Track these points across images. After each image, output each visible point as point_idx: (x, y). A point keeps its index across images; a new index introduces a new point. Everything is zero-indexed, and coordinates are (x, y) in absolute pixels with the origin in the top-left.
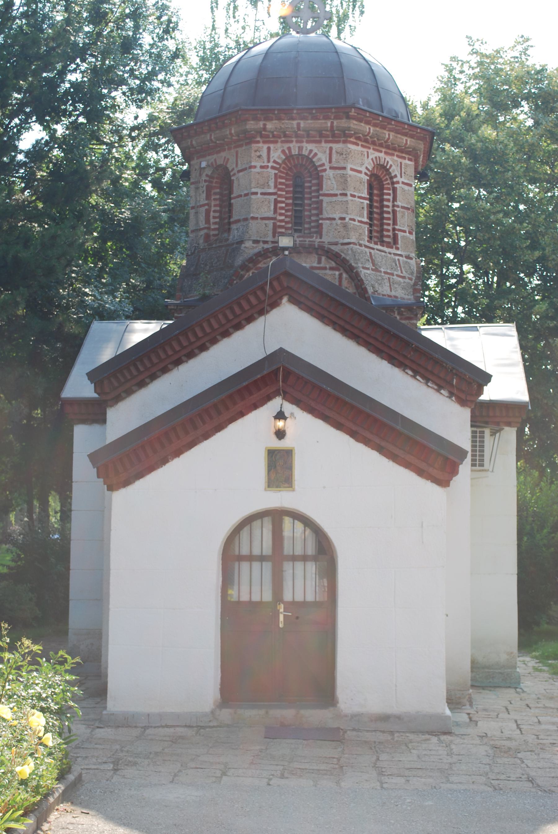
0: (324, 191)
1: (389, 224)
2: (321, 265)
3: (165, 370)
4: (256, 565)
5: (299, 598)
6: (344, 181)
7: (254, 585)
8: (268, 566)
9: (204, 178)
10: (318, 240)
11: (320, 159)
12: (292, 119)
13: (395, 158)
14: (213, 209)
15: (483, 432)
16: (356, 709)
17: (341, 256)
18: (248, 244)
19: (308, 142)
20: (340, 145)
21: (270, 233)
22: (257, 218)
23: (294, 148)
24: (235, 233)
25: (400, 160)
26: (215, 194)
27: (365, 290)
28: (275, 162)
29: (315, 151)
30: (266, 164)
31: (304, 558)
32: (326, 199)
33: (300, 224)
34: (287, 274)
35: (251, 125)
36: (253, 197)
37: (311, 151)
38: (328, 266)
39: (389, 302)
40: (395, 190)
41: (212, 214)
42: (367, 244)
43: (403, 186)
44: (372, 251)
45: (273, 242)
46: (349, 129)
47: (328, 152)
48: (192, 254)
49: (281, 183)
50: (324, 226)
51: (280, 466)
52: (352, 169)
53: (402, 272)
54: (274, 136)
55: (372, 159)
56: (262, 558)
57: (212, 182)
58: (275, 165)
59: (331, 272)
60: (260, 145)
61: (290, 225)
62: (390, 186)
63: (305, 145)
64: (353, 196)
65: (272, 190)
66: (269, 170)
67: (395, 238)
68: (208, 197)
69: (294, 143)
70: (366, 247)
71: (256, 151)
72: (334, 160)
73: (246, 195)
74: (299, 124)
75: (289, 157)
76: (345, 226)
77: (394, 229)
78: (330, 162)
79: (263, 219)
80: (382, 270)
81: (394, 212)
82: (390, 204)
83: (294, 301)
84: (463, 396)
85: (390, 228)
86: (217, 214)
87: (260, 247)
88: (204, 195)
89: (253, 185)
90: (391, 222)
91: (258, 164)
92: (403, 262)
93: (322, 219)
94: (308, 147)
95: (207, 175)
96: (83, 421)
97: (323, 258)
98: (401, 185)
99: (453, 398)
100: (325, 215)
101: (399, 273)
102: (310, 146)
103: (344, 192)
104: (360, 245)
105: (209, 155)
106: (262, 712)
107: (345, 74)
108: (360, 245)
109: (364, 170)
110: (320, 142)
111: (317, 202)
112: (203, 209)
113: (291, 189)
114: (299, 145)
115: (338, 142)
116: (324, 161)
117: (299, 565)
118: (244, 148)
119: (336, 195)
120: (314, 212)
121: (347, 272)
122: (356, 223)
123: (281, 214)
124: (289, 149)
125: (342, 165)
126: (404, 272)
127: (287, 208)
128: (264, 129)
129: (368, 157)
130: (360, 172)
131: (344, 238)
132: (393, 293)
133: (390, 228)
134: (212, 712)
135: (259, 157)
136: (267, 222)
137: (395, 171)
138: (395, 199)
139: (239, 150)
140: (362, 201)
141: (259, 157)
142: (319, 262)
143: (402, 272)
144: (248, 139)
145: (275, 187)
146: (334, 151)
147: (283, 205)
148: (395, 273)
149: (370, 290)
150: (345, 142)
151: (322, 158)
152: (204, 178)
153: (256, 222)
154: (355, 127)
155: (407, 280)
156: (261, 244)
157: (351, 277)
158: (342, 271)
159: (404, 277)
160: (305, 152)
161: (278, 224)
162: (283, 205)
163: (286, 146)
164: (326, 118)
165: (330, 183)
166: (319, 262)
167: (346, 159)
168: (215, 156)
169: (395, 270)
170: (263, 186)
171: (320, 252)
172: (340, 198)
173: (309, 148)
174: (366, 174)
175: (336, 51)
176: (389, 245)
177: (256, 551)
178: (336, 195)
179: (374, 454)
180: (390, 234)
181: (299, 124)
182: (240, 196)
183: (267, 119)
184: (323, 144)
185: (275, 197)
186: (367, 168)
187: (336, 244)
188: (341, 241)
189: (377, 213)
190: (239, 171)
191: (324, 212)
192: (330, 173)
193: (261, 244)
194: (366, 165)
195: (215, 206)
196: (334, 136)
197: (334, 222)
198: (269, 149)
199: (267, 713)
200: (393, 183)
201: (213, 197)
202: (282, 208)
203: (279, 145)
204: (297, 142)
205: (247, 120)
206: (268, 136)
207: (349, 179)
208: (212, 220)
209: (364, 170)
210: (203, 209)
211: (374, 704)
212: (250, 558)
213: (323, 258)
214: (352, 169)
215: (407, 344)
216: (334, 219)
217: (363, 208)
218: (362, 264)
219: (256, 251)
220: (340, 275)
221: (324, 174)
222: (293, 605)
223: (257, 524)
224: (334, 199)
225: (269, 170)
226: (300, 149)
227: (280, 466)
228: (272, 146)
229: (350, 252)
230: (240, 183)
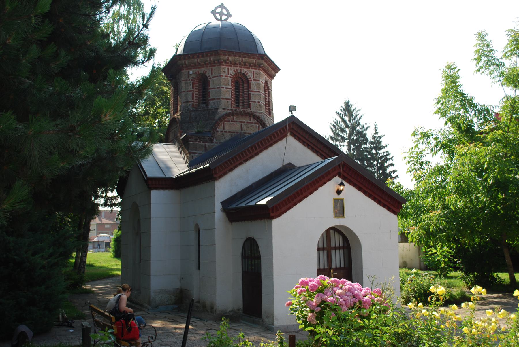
3: (241, 164)
5: (338, 266)
9: (191, 78)
11: (249, 76)
12: (240, 57)
14: (195, 93)
18: (221, 110)
19: (244, 68)
20: (257, 71)
23: (239, 69)
24: (212, 104)
26: (196, 86)
29: (247, 72)
31: (339, 248)
35: (222, 57)
41: (195, 95)
46: (262, 64)
48: (185, 112)
50: (252, 105)
51: (339, 208)
54: (231, 63)
59: (255, 125)
60: (225, 66)
63: (243, 68)
65: (230, 87)
68: (193, 88)
74: (242, 59)
75: (237, 73)
79: (227, 99)
86: (197, 96)
87: (225, 112)
88: (191, 86)
89: (222, 84)
91: (224, 75)
94: (245, 70)
95: (193, 78)
96: (156, 188)
97: (252, 118)
102: (245, 70)
105: (194, 68)
110: (249, 68)
112: (191, 93)
115: (256, 69)
117: (337, 251)
118: (216, 67)
125: (258, 79)
128: (228, 60)
139: (213, 68)
141: (224, 72)
142: (250, 120)
144: (219, 63)
150: (259, 69)
151: (250, 75)
152: (191, 78)
160: (243, 72)
163: (235, 68)
164: (254, 58)
165: (253, 86)
166: (250, 120)
167: (259, 77)
170: (226, 85)
172: (257, 93)
177: (337, 245)
179: (372, 201)
181: (242, 59)
183: (230, 55)
184: (250, 69)
187: (257, 113)
190: (213, 77)
196: (255, 66)
198: (228, 69)
203: (232, 67)
205: (221, 55)
206: (228, 63)
208: (195, 98)
210: (191, 93)
213: (252, 118)
219: (225, 113)
220: (259, 126)
224: (255, 93)
226: (241, 70)
227: (339, 208)
230: (213, 83)
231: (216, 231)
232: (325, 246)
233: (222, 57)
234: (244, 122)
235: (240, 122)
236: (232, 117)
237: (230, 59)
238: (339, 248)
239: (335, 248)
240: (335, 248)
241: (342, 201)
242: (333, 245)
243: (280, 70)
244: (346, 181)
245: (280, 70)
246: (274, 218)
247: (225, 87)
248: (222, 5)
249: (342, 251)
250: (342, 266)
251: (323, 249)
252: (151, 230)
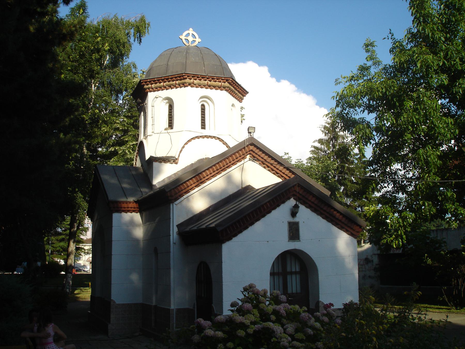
31: (296, 273)
51: (294, 232)
164: (173, 81)
177: (293, 270)
181: (208, 82)
227: (294, 232)
231: (172, 254)
232: (280, 271)
237: (195, 82)
238: (296, 273)
239: (291, 273)
241: (297, 224)
242: (289, 269)
243: (248, 93)
244: (301, 204)
245: (248, 93)
246: (224, 241)
249: (298, 276)
250: (299, 291)
251: (278, 274)
252: (113, 254)
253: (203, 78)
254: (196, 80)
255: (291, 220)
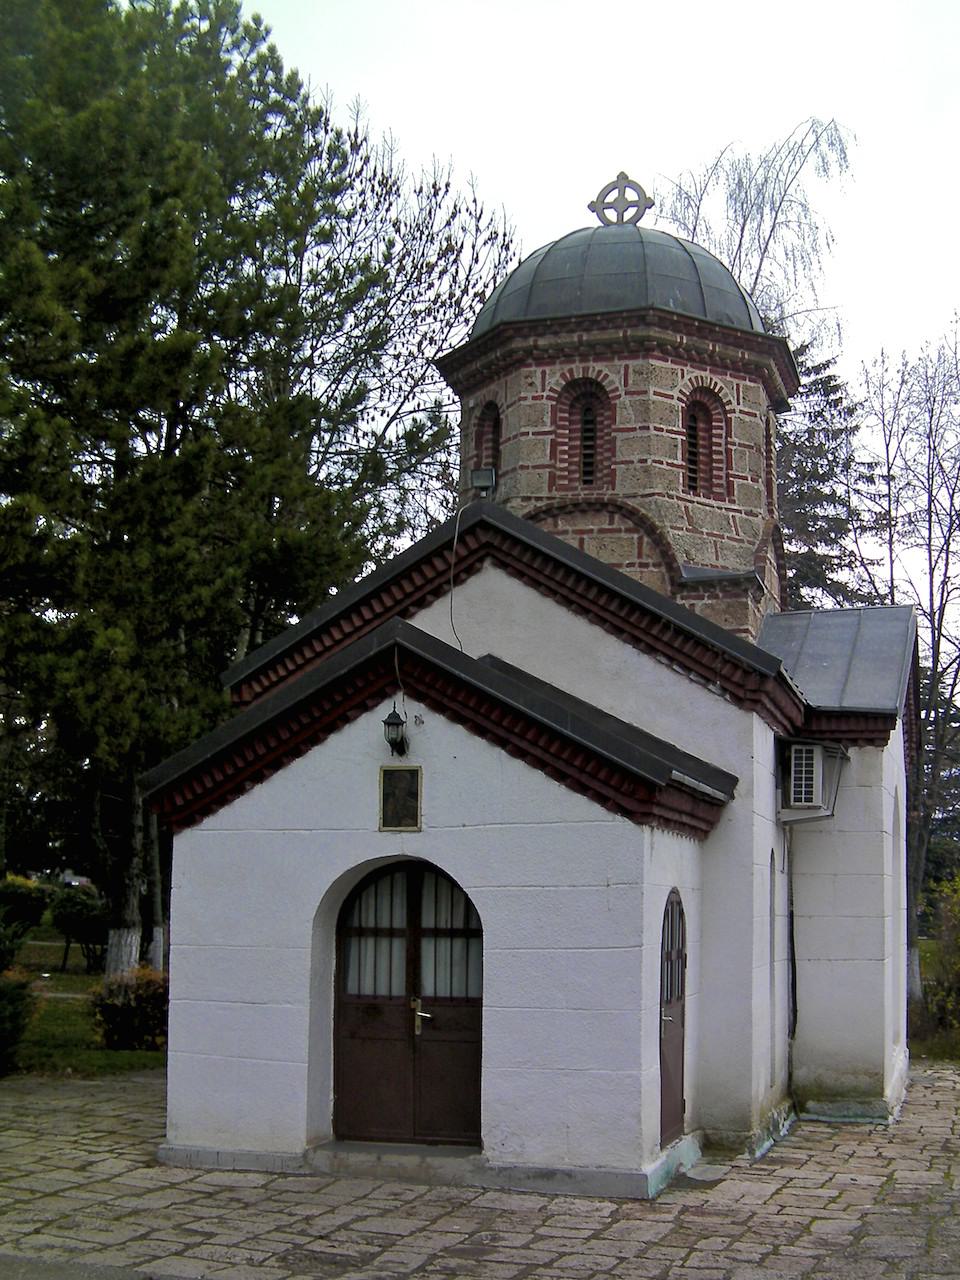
0: (619, 425)
1: (721, 469)
2: (614, 526)
4: (384, 943)
6: (644, 409)
7: (379, 971)
8: (459, 943)
10: (610, 492)
11: (612, 382)
13: (728, 378)
14: (484, 461)
15: (811, 752)
16: (510, 1160)
17: (639, 511)
19: (595, 360)
20: (640, 362)
21: (545, 486)
22: (528, 467)
25: (735, 381)
26: (487, 441)
27: (673, 558)
28: (551, 390)
29: (606, 371)
30: (540, 394)
32: (620, 436)
33: (590, 473)
34: (484, 525)
36: (523, 438)
37: (600, 372)
38: (623, 528)
39: (714, 573)
40: (728, 422)
42: (682, 495)
43: (741, 416)
44: (688, 504)
45: (548, 498)
46: (649, 339)
47: (622, 372)
49: (562, 419)
51: (401, 799)
52: (655, 393)
53: (737, 534)
55: (690, 380)
56: (391, 933)
57: (483, 426)
58: (552, 394)
60: (533, 369)
61: (577, 476)
62: (722, 417)
64: (656, 429)
65: (547, 429)
66: (544, 401)
67: (730, 487)
69: (577, 363)
70: (678, 498)
71: (526, 377)
72: (630, 382)
73: (515, 437)
74: (580, 337)
76: (646, 471)
77: (728, 475)
78: (626, 384)
79: (535, 467)
80: (705, 530)
81: (728, 451)
82: (722, 441)
83: (501, 564)
84: (741, 694)
85: (722, 474)
87: (530, 507)
90: (723, 466)
92: (741, 519)
93: (616, 463)
98: (737, 414)
99: (728, 697)
100: (619, 457)
101: (734, 535)
102: (599, 366)
103: (646, 424)
104: (671, 497)
106: (372, 1158)
107: (648, 269)
108: (671, 497)
109: (676, 393)
111: (609, 442)
113: (579, 426)
114: (584, 365)
116: (617, 384)
117: (444, 944)
119: (634, 429)
120: (607, 455)
121: (649, 535)
122: (664, 466)
123: (563, 461)
124: (571, 371)
126: (741, 534)
127: (572, 452)
129: (683, 377)
130: (672, 397)
131: (645, 487)
132: (721, 562)
133: (722, 474)
134: (305, 1155)
135: (531, 384)
136: (540, 471)
137: (728, 395)
138: (729, 434)
140: (674, 436)
142: (611, 522)
143: (737, 534)
145: (553, 422)
146: (631, 370)
147: (566, 448)
148: (726, 534)
149: (681, 559)
150: (645, 357)
153: (526, 471)
154: (657, 335)
155: (746, 545)
156: (533, 501)
157: (654, 541)
158: (642, 532)
159: (742, 541)
160: (592, 375)
161: (558, 473)
162: (566, 448)
163: (567, 367)
168: (484, 391)
169: (727, 531)
170: (669, 423)
171: (610, 508)
172: (639, 433)
173: (597, 369)
174: (679, 399)
175: (641, 240)
176: (719, 497)
177: (385, 923)
178: (634, 429)
180: (723, 482)
181: (580, 337)
182: (509, 439)
185: (553, 437)
186: (681, 391)
188: (642, 492)
189: (704, 454)
190: (508, 407)
191: (618, 453)
192: (626, 399)
193: (533, 501)
194: (679, 387)
195: (487, 457)
197: (631, 466)
198: (544, 373)
199: (379, 1159)
200: (726, 412)
201: (484, 446)
202: (564, 452)
203: (558, 367)
204: (581, 361)
207: (652, 407)
209: (676, 393)
211: (537, 1155)
212: (377, 933)
214: (655, 393)
215: (656, 618)
216: (632, 462)
217: (676, 446)
218: (670, 521)
220: (640, 539)
221: (617, 401)
222: (431, 1003)
223: (385, 886)
224: (632, 434)
225: (544, 401)
226: (586, 370)
227: (401, 799)
228: (548, 369)
229: (653, 507)
233: (518, 343)
234: (591, 531)
235: (574, 532)
236: (550, 520)
237: (542, 342)
240: (437, 933)
241: (414, 774)
242: (428, 921)
247: (531, 430)
248: (623, 176)
253: (563, 325)
254: (541, 335)
255: (397, 763)
